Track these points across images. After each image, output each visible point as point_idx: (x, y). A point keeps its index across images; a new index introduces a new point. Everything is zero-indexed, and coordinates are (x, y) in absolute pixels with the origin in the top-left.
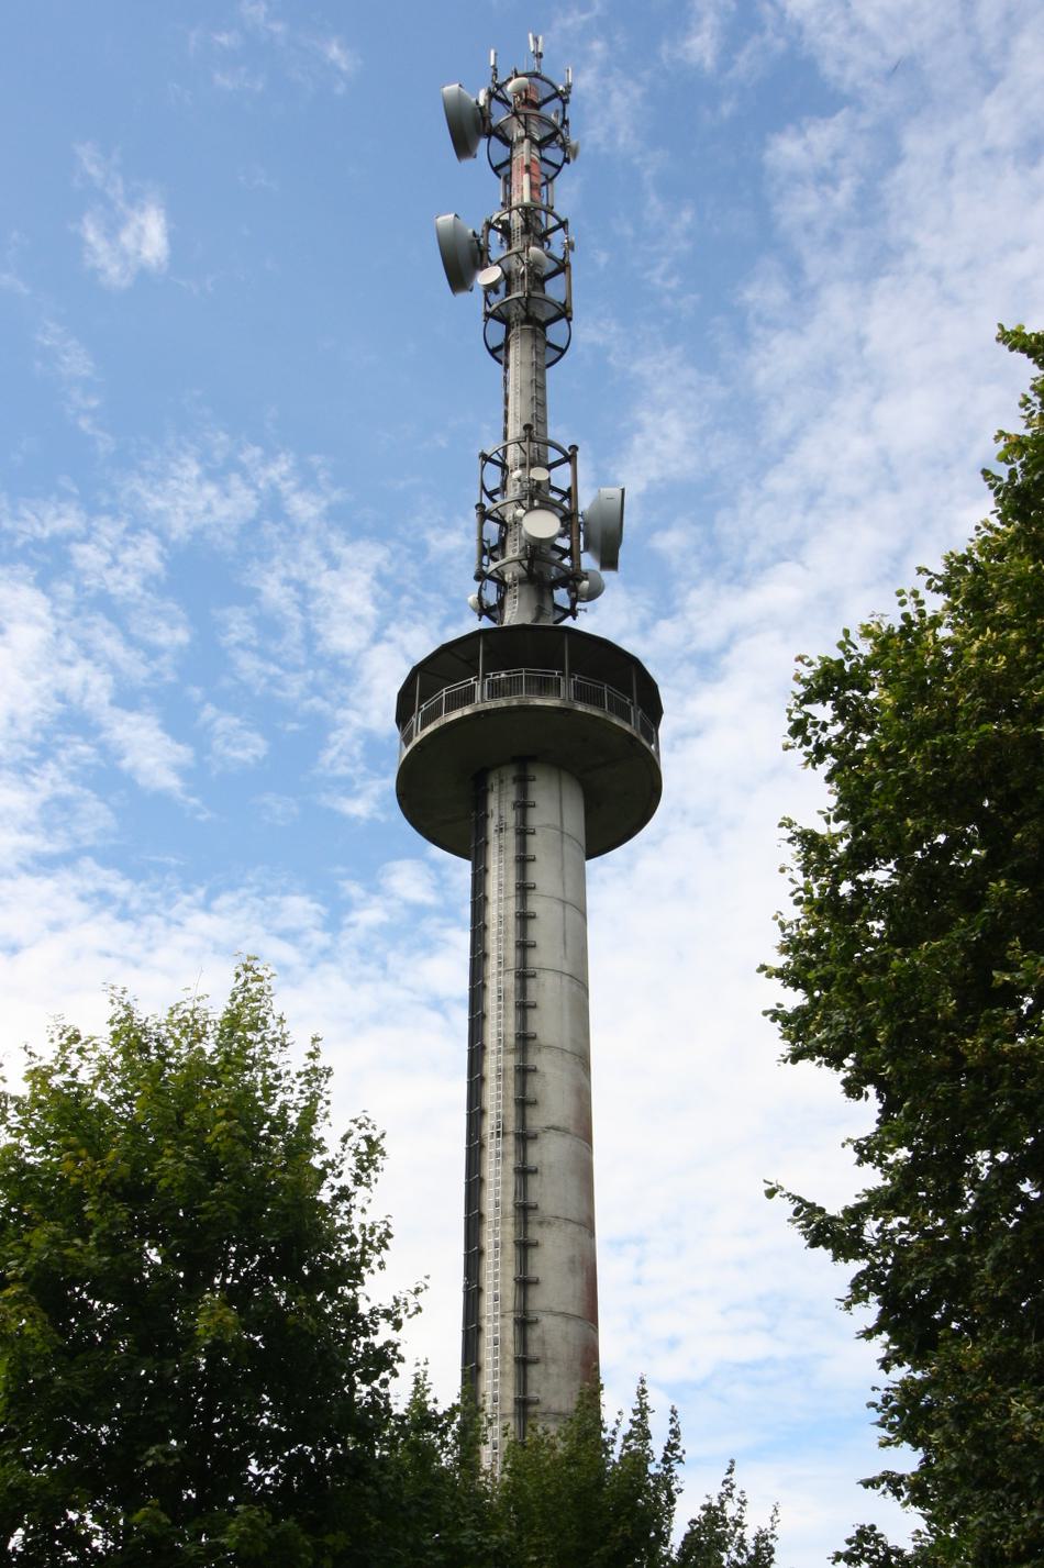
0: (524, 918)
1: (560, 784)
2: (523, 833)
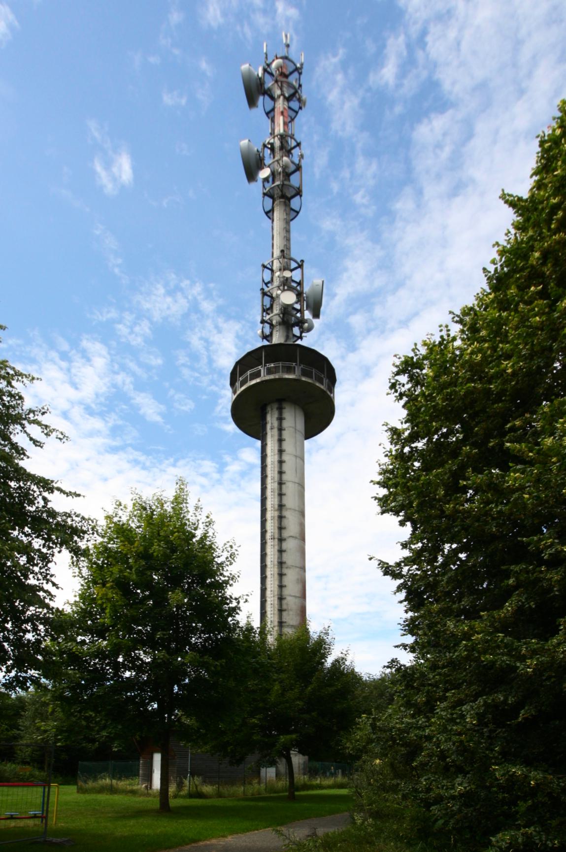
1: (295, 417)
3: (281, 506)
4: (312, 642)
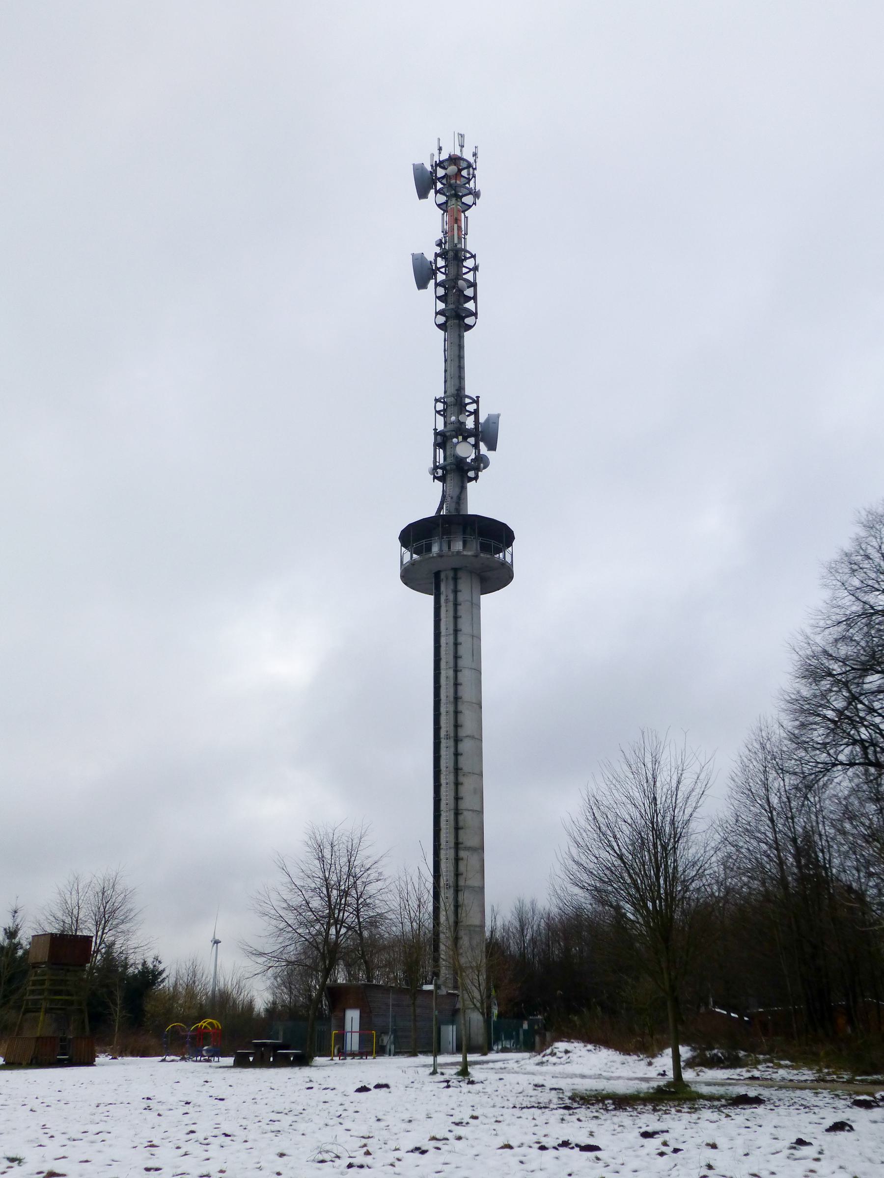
0: (456, 644)
1: (471, 580)
2: (456, 605)
3: (457, 699)
4: (517, 955)
